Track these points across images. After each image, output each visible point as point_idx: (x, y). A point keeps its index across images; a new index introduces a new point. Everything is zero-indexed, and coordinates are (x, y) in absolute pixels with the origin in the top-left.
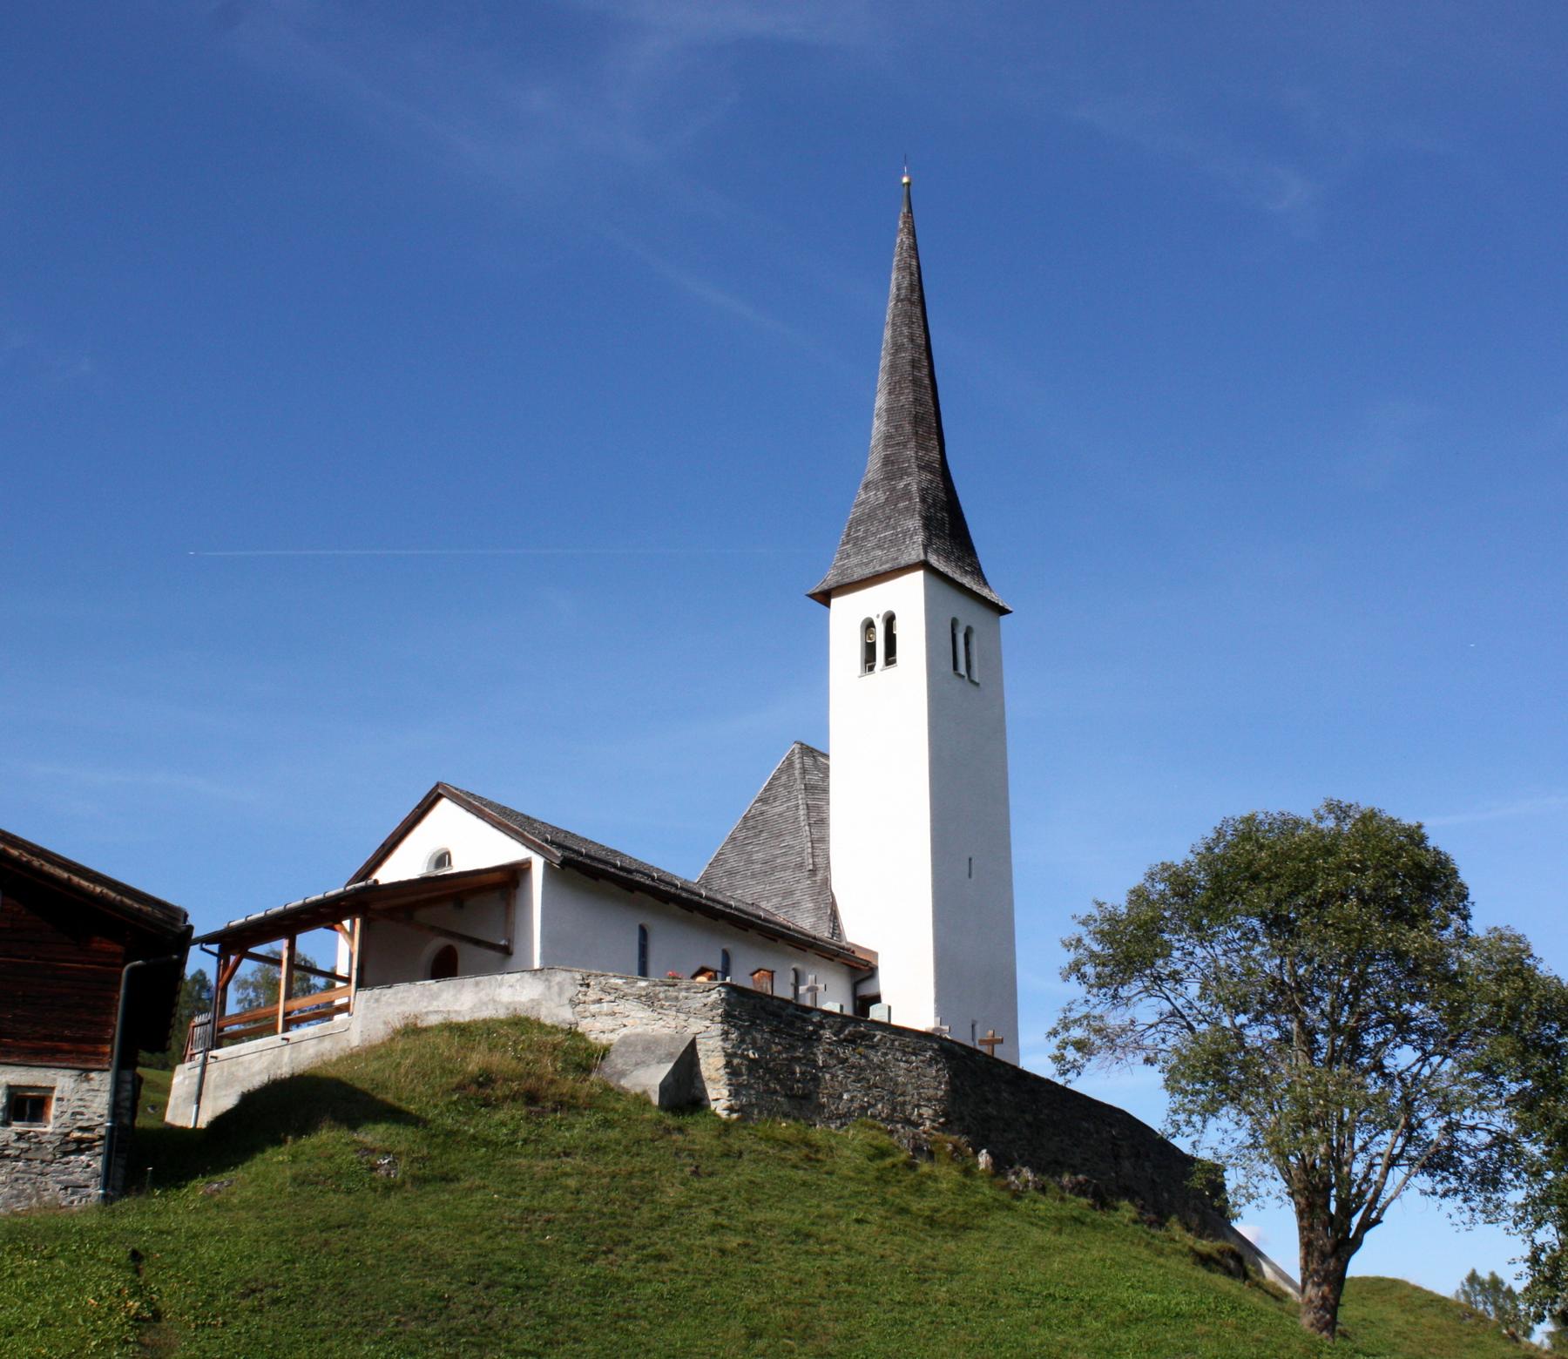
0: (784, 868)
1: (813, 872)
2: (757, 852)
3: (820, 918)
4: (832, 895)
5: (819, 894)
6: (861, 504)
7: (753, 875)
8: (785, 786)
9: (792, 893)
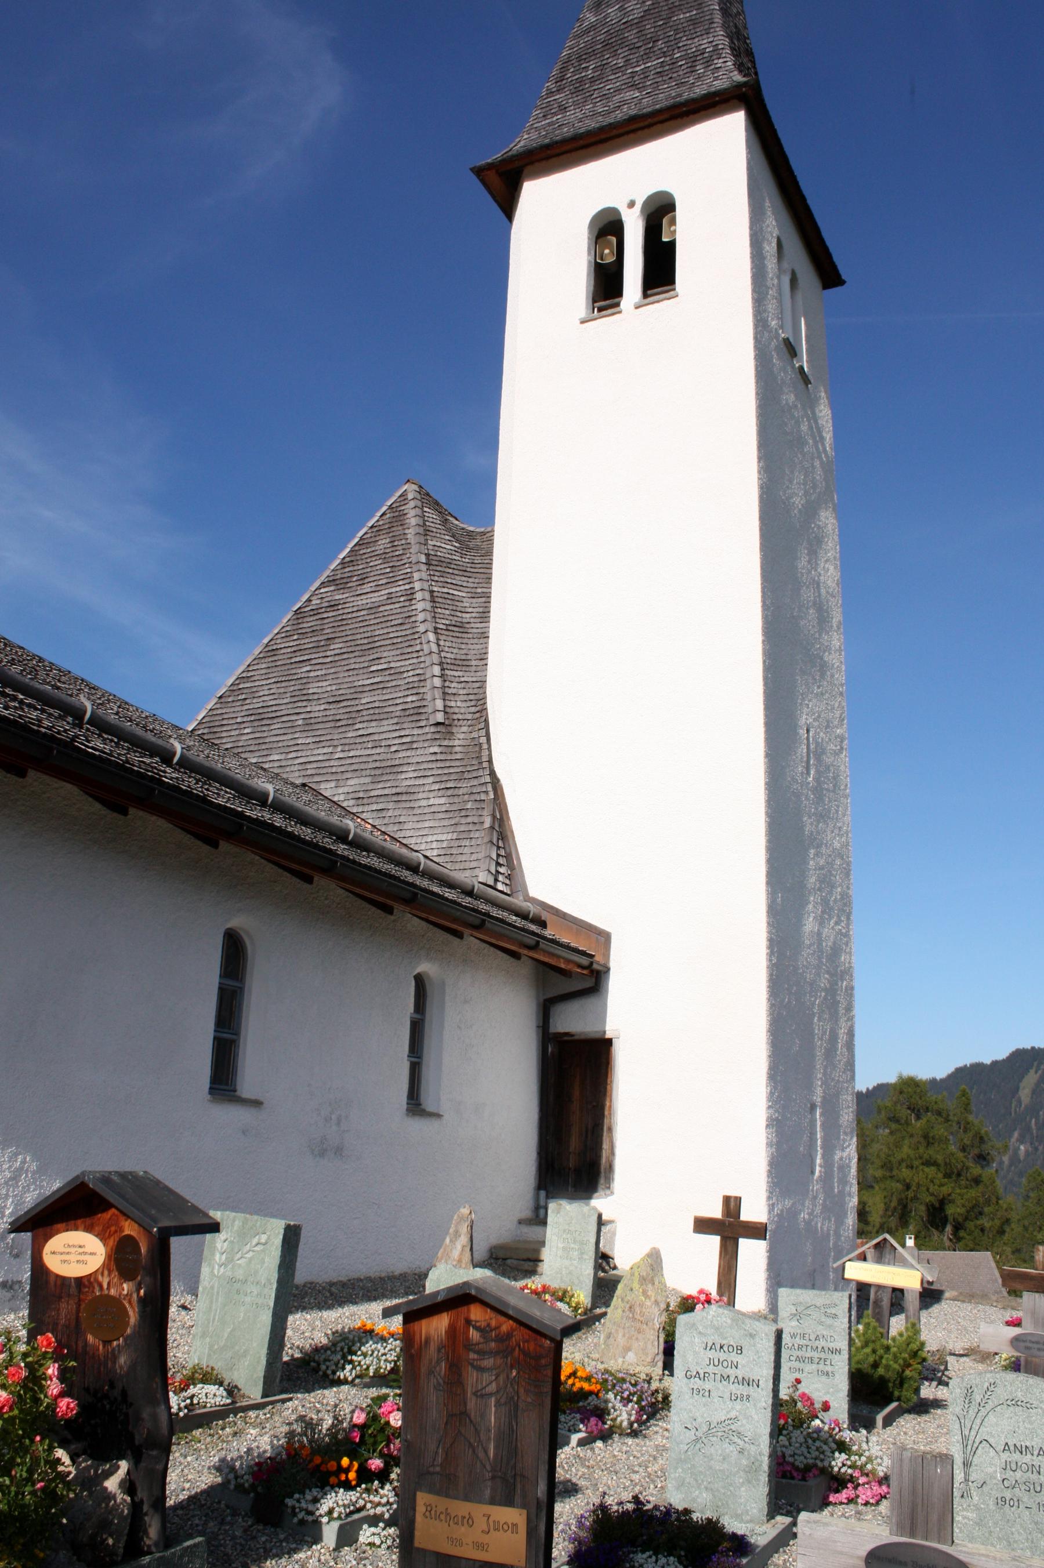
0: (378, 714)
1: (445, 727)
2: (319, 679)
3: (464, 836)
4: (495, 782)
5: (461, 776)
6: (587, 31)
7: (309, 725)
8: (384, 557)
9: (394, 769)
